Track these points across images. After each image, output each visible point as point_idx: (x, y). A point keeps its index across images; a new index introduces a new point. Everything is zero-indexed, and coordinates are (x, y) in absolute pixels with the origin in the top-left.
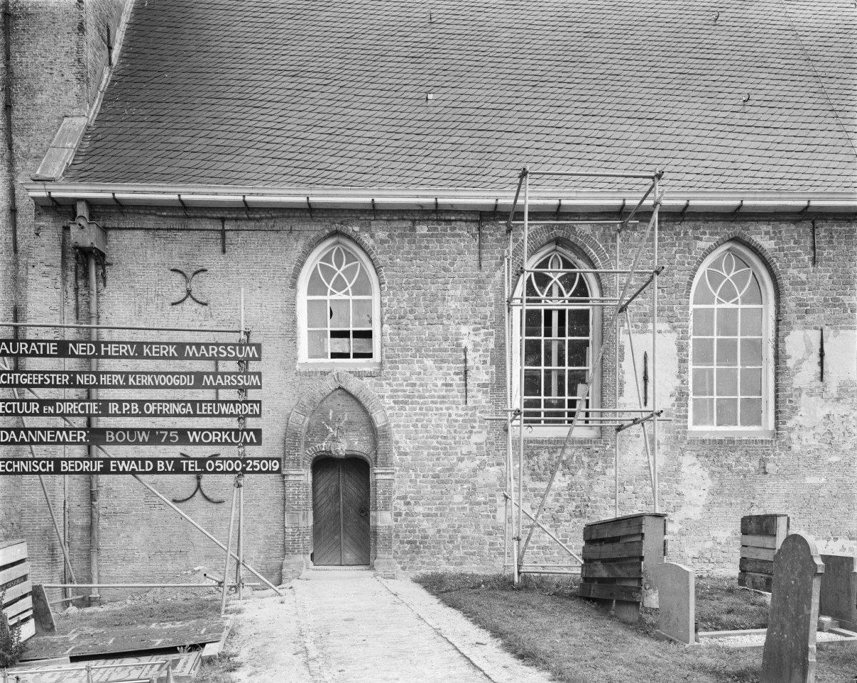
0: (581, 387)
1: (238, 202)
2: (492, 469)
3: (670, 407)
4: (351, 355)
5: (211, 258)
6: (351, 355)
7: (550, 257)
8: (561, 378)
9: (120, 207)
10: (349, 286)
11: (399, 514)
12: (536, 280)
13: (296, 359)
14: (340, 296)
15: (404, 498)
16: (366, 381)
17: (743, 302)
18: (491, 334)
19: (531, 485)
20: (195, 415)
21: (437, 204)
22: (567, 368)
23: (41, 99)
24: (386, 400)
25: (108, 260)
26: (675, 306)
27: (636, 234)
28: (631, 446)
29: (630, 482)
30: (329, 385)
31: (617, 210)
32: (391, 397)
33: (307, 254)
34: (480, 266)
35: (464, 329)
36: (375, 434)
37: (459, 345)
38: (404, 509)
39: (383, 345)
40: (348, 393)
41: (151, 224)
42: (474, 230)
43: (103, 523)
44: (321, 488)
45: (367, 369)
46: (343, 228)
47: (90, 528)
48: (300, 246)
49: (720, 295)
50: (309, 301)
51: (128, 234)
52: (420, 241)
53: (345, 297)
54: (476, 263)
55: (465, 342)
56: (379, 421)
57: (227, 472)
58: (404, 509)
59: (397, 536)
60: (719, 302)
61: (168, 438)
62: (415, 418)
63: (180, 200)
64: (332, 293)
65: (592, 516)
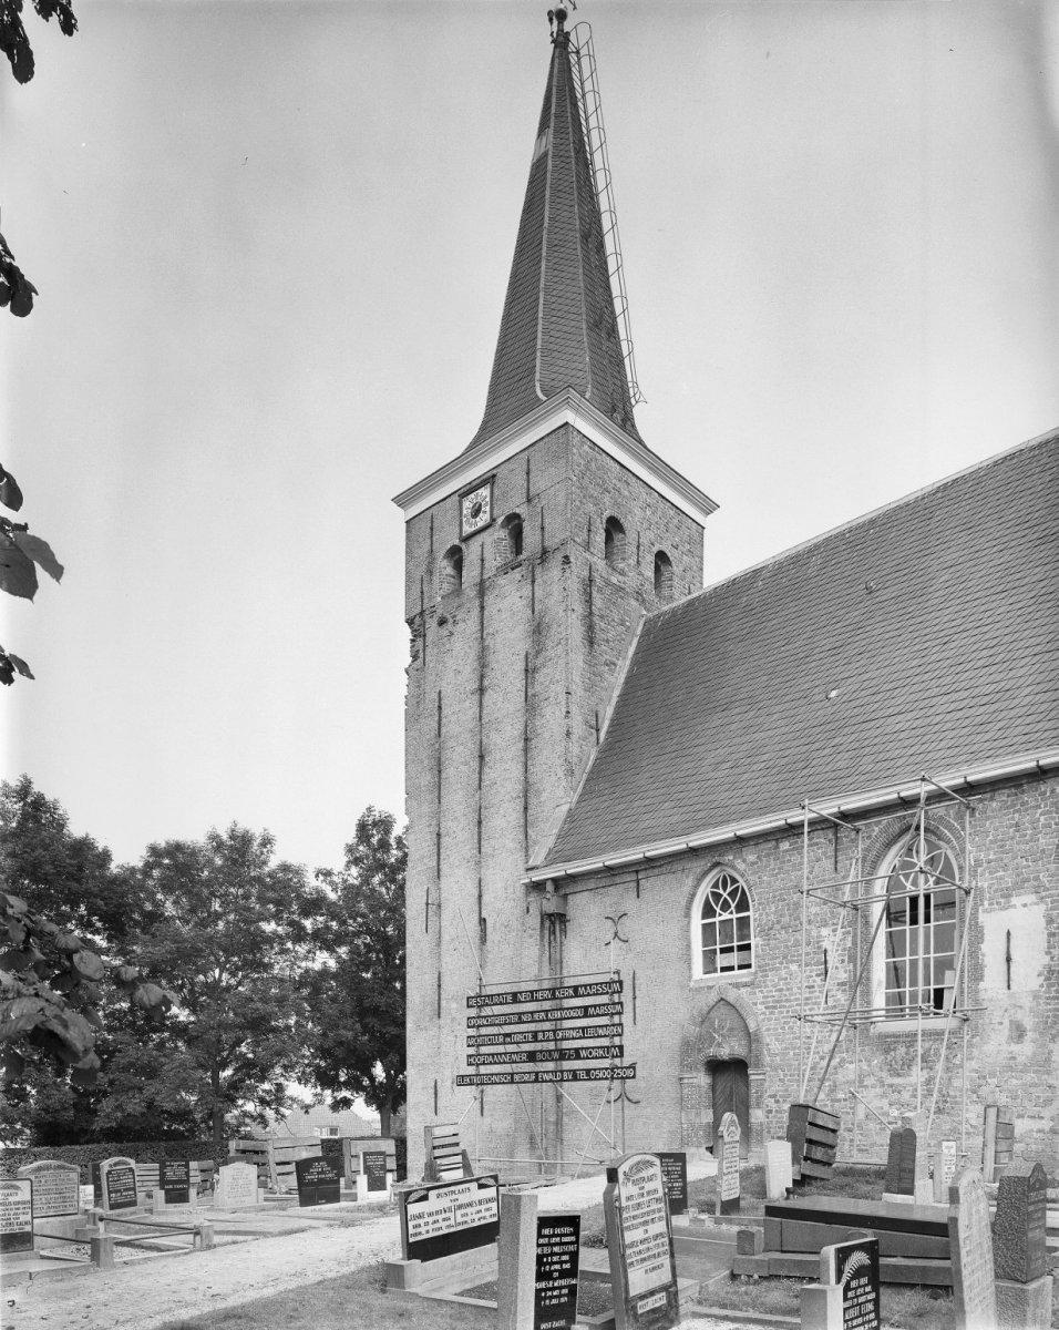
0: (948, 974)
2: (852, 1066)
3: (1037, 988)
4: (736, 967)
5: (630, 904)
6: (736, 967)
8: (927, 966)
9: (572, 878)
10: (733, 905)
11: (770, 1111)
13: (690, 977)
14: (726, 916)
15: (774, 1096)
16: (742, 990)
18: (848, 933)
19: (890, 1080)
20: (584, 1038)
22: (932, 955)
23: (544, 796)
24: (759, 1006)
25: (568, 918)
26: (1041, 875)
27: (994, 804)
28: (993, 1035)
29: (993, 1075)
30: (713, 997)
32: (763, 1003)
33: (696, 887)
34: (836, 869)
35: (825, 932)
36: (751, 1038)
37: (819, 947)
38: (774, 1106)
39: (756, 956)
40: (729, 1004)
41: (593, 886)
42: (831, 836)
43: (565, 1119)
44: (719, 1088)
45: (744, 980)
46: (721, 860)
47: (559, 1123)
48: (690, 882)
50: (703, 925)
51: (579, 896)
52: (783, 857)
53: (730, 917)
54: (833, 866)
55: (826, 944)
56: (752, 1027)
57: (602, 1079)
58: (774, 1106)
59: (769, 1132)
61: (570, 1055)
62: (782, 1021)
64: (720, 915)
65: (952, 1112)
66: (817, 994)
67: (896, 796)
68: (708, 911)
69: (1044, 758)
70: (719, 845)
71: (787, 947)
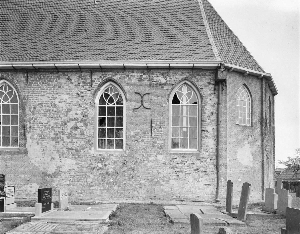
1: (77, 66)
7: (109, 88)
10: (10, 99)
12: (105, 96)
17: (11, 102)
21: (170, 66)
31: (192, 68)
49: (108, 102)
60: (108, 104)
63: (79, 66)
67: (99, 65)
68: (102, 101)
69: (57, 64)
70: (69, 69)
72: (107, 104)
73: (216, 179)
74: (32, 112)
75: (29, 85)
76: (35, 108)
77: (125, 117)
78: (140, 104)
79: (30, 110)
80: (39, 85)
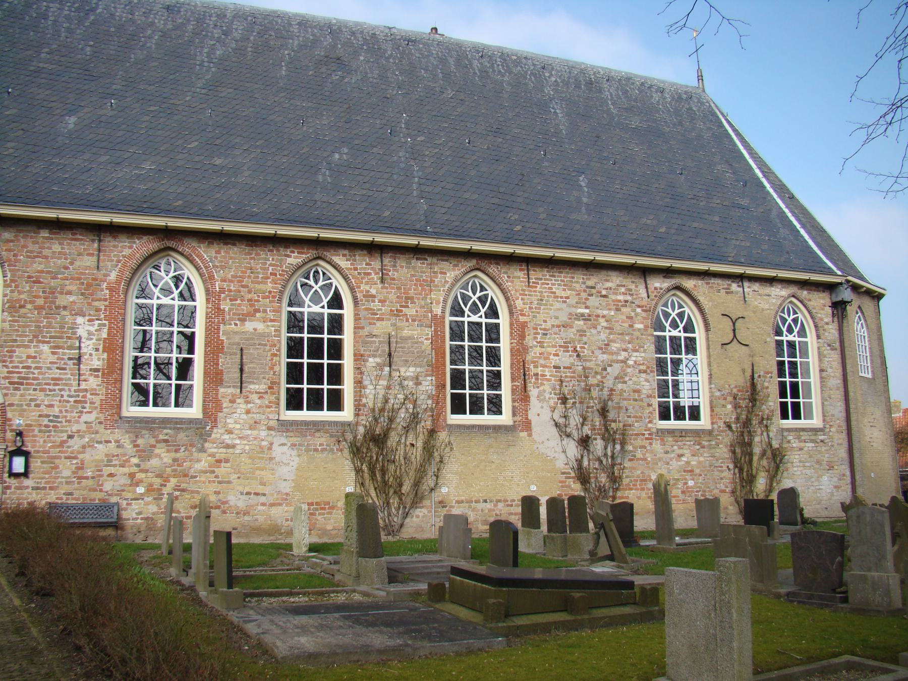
35: (80, 320)
53: (479, 320)
66: (69, 376)
71: (39, 327)
72: (155, 297)
73: (848, 473)
74: (539, 342)
75: (532, 287)
76: (544, 334)
77: (284, 360)
78: (731, 336)
79: (535, 338)
80: (551, 288)
